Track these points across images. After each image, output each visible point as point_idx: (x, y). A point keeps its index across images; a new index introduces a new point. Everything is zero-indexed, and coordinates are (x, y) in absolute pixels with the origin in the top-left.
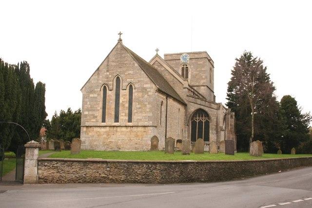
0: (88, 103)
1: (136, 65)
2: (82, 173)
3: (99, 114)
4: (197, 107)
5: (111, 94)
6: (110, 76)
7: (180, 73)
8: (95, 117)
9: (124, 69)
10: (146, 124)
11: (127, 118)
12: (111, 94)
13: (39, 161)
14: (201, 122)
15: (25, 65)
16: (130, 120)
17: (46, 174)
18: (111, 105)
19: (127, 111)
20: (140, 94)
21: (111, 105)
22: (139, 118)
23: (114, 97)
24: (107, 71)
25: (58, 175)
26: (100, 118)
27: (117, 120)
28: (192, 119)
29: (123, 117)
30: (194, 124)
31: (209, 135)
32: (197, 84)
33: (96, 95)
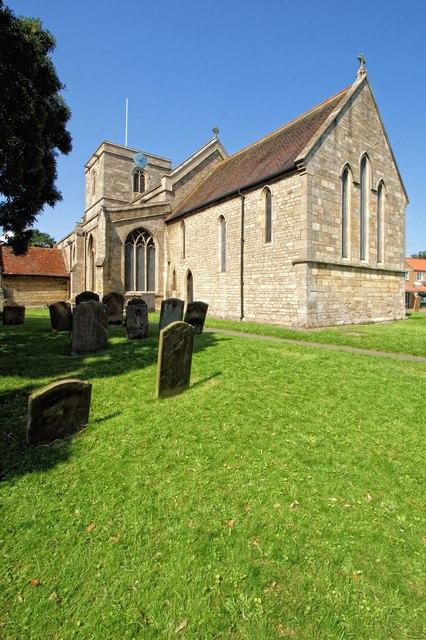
8: (332, 242)
22: (392, 254)
33: (332, 187)
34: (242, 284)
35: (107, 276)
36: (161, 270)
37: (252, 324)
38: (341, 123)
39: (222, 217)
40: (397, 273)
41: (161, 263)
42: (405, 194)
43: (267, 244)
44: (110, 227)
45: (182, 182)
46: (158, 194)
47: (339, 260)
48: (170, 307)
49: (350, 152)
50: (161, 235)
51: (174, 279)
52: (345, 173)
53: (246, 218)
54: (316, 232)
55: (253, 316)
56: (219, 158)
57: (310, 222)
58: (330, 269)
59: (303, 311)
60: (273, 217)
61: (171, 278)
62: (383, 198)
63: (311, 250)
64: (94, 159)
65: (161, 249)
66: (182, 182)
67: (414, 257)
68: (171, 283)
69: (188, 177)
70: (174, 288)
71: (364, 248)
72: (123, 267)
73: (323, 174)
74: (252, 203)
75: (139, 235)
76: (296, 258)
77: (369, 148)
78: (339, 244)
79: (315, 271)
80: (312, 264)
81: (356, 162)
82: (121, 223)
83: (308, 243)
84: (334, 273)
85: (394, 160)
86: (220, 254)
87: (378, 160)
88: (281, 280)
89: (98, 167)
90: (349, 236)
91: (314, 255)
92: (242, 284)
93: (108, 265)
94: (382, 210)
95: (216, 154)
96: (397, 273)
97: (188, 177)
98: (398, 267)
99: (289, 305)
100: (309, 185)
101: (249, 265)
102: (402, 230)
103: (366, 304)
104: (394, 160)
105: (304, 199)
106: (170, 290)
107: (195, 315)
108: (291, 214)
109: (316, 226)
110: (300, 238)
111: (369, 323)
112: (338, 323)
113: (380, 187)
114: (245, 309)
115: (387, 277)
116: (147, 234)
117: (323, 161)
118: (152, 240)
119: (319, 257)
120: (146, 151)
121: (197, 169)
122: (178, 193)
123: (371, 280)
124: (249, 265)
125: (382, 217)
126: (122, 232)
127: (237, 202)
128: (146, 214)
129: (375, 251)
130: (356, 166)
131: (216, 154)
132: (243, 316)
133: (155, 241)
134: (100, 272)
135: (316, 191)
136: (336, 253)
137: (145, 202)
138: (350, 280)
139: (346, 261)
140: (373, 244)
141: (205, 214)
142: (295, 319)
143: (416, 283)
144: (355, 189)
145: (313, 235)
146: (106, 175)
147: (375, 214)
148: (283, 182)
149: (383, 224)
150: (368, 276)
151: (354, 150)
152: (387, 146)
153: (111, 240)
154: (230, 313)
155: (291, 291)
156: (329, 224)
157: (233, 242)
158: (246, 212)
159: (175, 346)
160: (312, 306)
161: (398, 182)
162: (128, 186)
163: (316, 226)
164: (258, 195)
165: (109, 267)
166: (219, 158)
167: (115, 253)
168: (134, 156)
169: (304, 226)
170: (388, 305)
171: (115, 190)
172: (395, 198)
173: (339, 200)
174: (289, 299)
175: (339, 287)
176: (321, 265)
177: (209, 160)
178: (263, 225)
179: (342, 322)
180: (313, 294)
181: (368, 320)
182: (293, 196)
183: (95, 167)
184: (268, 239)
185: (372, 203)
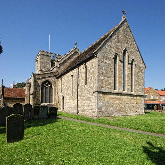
0: (103, 68)
8: (110, 84)
22: (138, 89)
33: (110, 62)
34: (78, 101)
35: (34, 98)
36: (55, 95)
37: (81, 115)
38: (114, 37)
39: (72, 76)
40: (140, 96)
41: (55, 93)
42: (145, 64)
43: (85, 85)
44: (35, 80)
45: (63, 63)
46: (54, 68)
47: (113, 91)
48: (42, 109)
49: (118, 49)
50: (55, 82)
51: (59, 99)
52: (115, 58)
53: (79, 76)
54: (102, 80)
55: (81, 112)
56: (77, 54)
57: (99, 76)
58: (108, 94)
59: (96, 110)
60: (87, 75)
61: (58, 99)
62: (134, 66)
63: (100, 87)
64: (38, 56)
65: (55, 88)
66: (63, 63)
67: (162, 90)
68: (58, 100)
69: (65, 61)
70: (59, 102)
71: (125, 86)
72: (40, 94)
73: (106, 57)
74: (81, 70)
75: (47, 83)
76: (94, 90)
77: (127, 47)
78: (113, 85)
79: (101, 95)
80: (99, 92)
81: (121, 52)
82: (40, 79)
83: (98, 85)
84: (111, 96)
85: (139, 51)
86: (72, 89)
87: (132, 51)
88: (90, 99)
89: (39, 60)
90: (117, 82)
91: (101, 89)
92: (78, 101)
93: (34, 94)
94: (134, 71)
95: (76, 53)
96: (140, 96)
97: (65, 61)
98: (141, 94)
99: (92, 109)
100: (99, 62)
101: (80, 93)
102: (143, 79)
103: (125, 108)
104: (139, 51)
105: (97, 67)
106: (58, 103)
107: (53, 112)
108: (93, 74)
109: (102, 78)
110: (95, 83)
111: (126, 116)
112: (112, 115)
113: (132, 62)
114: (79, 110)
115: (135, 98)
116: (49, 83)
117: (106, 52)
118: (51, 85)
119: (103, 90)
120: (56, 53)
121: (69, 58)
122: (61, 68)
123: (128, 99)
124: (80, 93)
125: (134, 74)
126: (40, 82)
127: (76, 70)
128: (49, 75)
129: (130, 88)
130: (121, 54)
131: (76, 53)
132: (78, 113)
133: (52, 85)
134: (31, 96)
135: (102, 64)
136: (111, 88)
137: (51, 71)
138: (118, 99)
139: (116, 91)
140: (129, 84)
141: (67, 75)
142: (94, 114)
143: (161, 100)
144: (120, 63)
145: (100, 81)
146: (41, 62)
147: (130, 73)
148: (90, 61)
149: (134, 77)
150: (126, 97)
151: (120, 48)
152: (135, 46)
153: (36, 85)
154: (75, 111)
155: (92, 103)
156: (108, 77)
157: (75, 84)
158: (79, 74)
159: (14, 123)
160: (100, 109)
161: (141, 60)
162: (49, 66)
163: (102, 78)
164: (82, 67)
165: (35, 95)
166: (77, 54)
167: (38, 89)
168: (51, 55)
169: (96, 78)
170: (136, 109)
171: (44, 67)
172: (139, 66)
173: (113, 67)
174: (92, 106)
175: (113, 102)
176: (104, 93)
177: (73, 55)
178: (84, 78)
179: (114, 115)
180: (100, 104)
181: (126, 114)
182: (93, 66)
183: (38, 60)
184: (86, 84)
185: (128, 68)
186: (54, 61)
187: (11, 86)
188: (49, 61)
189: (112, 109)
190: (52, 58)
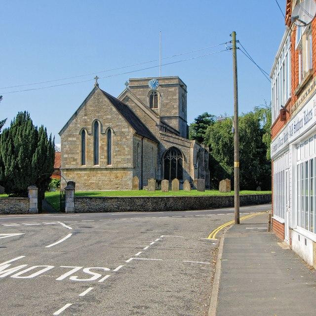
0: (67, 146)
1: (114, 109)
2: (102, 205)
3: (78, 157)
4: (172, 145)
5: (89, 139)
6: (88, 120)
7: (148, 105)
8: (75, 160)
9: (102, 114)
10: (125, 165)
11: (106, 160)
12: (89, 139)
13: (75, 198)
14: (174, 160)
15: (23, 120)
16: (109, 163)
17: (80, 207)
18: (89, 148)
19: (106, 154)
20: (119, 138)
21: (89, 148)
22: (119, 160)
23: (92, 141)
24: (85, 115)
25: (87, 207)
26: (79, 161)
27: (96, 162)
28: (165, 157)
29: (102, 159)
30: (167, 161)
31: (182, 173)
32: (168, 115)
33: (75, 139)
47: (80, 166)
186: (155, 93)
187: (263, 140)
188: (144, 97)
189: (79, 185)
190: (151, 87)
